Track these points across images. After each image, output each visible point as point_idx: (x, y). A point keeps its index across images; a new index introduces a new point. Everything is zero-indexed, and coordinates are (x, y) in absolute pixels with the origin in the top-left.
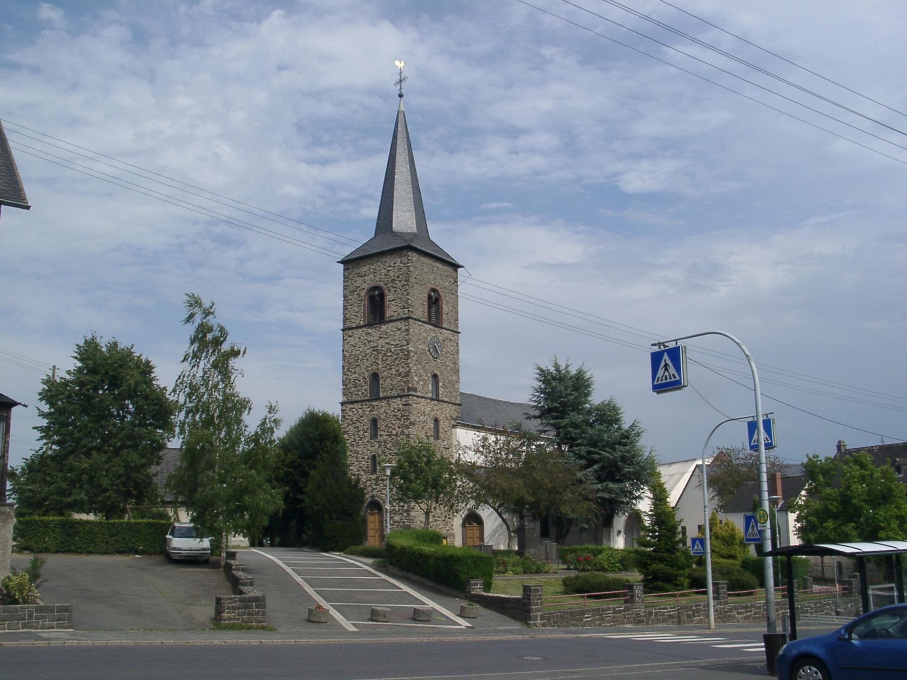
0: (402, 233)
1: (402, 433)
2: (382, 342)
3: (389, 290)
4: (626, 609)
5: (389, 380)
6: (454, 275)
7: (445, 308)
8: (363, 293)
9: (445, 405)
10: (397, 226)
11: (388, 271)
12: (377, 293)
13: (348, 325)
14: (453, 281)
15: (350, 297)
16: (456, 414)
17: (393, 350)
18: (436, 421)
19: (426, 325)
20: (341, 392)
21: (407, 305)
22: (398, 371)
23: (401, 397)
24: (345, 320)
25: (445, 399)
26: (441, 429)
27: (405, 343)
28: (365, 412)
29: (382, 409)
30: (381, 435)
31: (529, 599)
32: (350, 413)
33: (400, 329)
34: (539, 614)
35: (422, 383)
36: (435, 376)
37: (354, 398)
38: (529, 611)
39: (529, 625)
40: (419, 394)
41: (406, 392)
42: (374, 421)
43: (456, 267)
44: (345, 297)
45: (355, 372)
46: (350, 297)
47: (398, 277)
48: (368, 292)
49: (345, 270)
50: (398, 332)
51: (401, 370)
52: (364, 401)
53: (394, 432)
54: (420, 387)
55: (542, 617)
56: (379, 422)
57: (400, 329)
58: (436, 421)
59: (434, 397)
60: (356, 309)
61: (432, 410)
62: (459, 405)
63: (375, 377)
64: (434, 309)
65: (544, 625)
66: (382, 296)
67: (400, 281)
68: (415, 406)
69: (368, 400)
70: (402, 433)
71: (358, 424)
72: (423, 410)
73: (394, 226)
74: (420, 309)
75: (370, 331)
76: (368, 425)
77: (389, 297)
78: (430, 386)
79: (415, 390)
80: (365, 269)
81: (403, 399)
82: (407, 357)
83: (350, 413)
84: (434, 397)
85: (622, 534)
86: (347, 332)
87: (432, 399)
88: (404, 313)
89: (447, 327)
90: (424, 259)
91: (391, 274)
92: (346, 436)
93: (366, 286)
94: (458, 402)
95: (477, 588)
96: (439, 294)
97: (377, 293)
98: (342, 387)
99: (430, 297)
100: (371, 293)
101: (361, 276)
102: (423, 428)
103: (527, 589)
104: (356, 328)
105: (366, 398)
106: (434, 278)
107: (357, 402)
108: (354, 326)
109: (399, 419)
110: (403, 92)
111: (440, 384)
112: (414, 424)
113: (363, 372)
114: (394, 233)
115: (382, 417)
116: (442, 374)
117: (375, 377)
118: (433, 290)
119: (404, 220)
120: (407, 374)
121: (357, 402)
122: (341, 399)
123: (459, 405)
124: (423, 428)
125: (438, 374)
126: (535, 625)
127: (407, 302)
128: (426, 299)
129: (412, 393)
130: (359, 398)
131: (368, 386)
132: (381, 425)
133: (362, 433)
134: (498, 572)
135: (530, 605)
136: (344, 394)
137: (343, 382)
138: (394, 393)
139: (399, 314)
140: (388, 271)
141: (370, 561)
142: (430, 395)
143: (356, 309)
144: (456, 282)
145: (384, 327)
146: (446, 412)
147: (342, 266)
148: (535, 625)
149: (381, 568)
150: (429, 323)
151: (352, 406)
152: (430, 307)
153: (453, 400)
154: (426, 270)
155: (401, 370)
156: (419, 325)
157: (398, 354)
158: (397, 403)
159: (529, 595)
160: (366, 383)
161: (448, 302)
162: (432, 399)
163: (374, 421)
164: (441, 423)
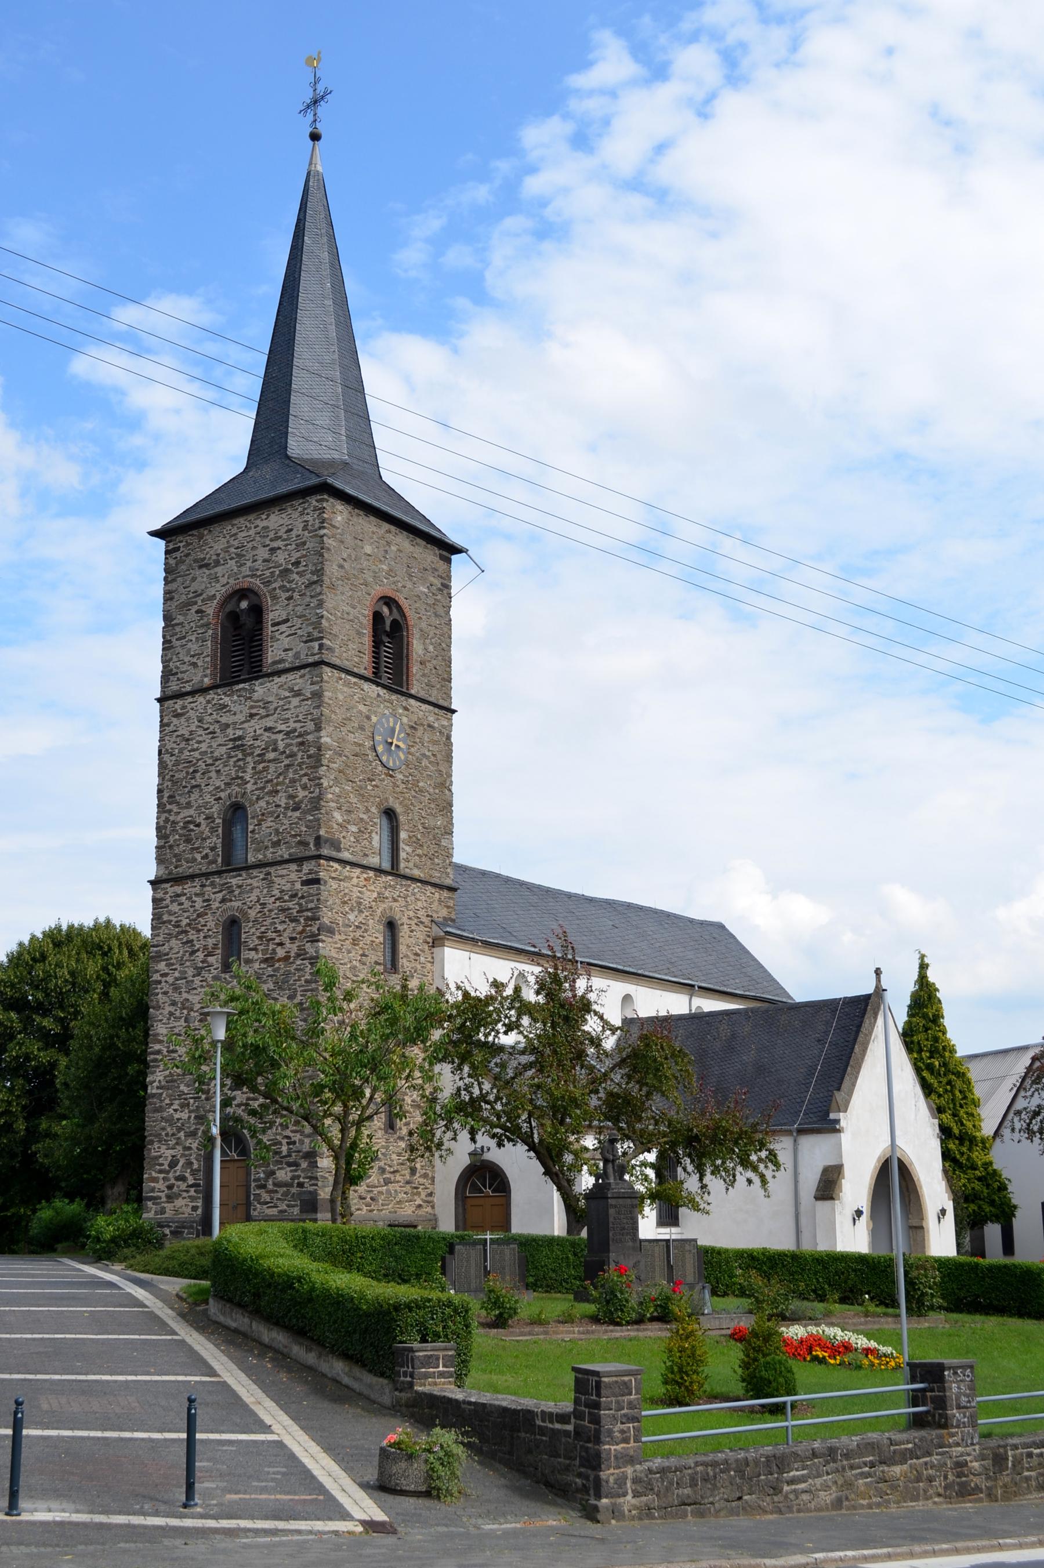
0: (314, 462)
1: (301, 954)
2: (256, 726)
3: (274, 598)
4: (922, 1450)
5: (269, 822)
6: (441, 565)
7: (417, 647)
8: (211, 609)
9: (415, 887)
10: (295, 447)
11: (273, 550)
12: (244, 605)
13: (174, 686)
14: (437, 582)
15: (180, 619)
16: (444, 913)
17: (281, 745)
18: (391, 926)
19: (366, 686)
20: (152, 853)
21: (316, 636)
22: (291, 797)
23: (299, 860)
24: (167, 675)
25: (416, 873)
26: (402, 949)
27: (311, 726)
28: (208, 904)
29: (252, 893)
30: (248, 961)
31: (596, 1420)
32: (175, 907)
33: (298, 694)
34: (629, 1470)
35: (354, 829)
36: (390, 814)
37: (184, 869)
38: (594, 1462)
39: (591, 1514)
40: (346, 855)
41: (312, 850)
42: (232, 926)
43: (448, 549)
44: (167, 618)
45: (189, 805)
46: (180, 619)
47: (297, 564)
48: (223, 604)
49: (167, 552)
50: (295, 701)
51: (301, 794)
52: (207, 875)
53: (281, 953)
54: (348, 840)
55: (643, 1486)
56: (246, 927)
57: (298, 694)
58: (391, 926)
59: (386, 865)
60: (194, 647)
61: (381, 898)
62: (452, 889)
63: (236, 811)
64: (386, 651)
65: (646, 1512)
66: (257, 611)
67: (301, 574)
68: (334, 885)
69: (219, 873)
70: (301, 954)
71: (192, 935)
72: (353, 899)
73: (292, 442)
74: (351, 642)
75: (226, 700)
76: (216, 939)
77: (273, 614)
78: (376, 838)
79: (336, 846)
80: (219, 547)
81: (306, 867)
82: (316, 761)
83: (175, 907)
84: (386, 865)
85: (864, 1218)
86: (167, 704)
87: (379, 871)
88: (306, 653)
89: (422, 694)
90: (369, 525)
91: (281, 557)
92: (162, 966)
93: (219, 591)
94: (448, 882)
95: (437, 1382)
96: (399, 608)
97: (244, 605)
98: (154, 841)
99: (377, 617)
100: (229, 608)
101: (207, 566)
102: (355, 942)
103: (587, 1384)
104: (192, 693)
105: (213, 868)
106: (390, 572)
107: (192, 877)
108: (188, 688)
109: (294, 920)
110: (321, 128)
111: (403, 835)
112: (331, 931)
113: (207, 803)
114: (288, 458)
115: (252, 914)
116: (407, 810)
117: (236, 811)
118: (388, 601)
119: (312, 438)
120: (316, 803)
121: (192, 877)
122: (151, 871)
123: (452, 889)
124: (355, 942)
125: (399, 809)
126: (616, 1512)
127: (317, 625)
128: (367, 622)
129: (325, 851)
130: (195, 869)
131: (221, 830)
132: (250, 934)
133: (200, 955)
134: (1008, 1247)
135: (598, 1440)
136: (160, 860)
137: (159, 829)
138: (284, 853)
139: (297, 655)
140: (273, 550)
141: (175, 1285)
142: (374, 861)
143: (194, 647)
144: (448, 587)
145: (261, 689)
146: (415, 906)
147: (161, 544)
148: (616, 1512)
149: (192, 1309)
150: (375, 679)
151: (178, 889)
152: (377, 644)
153: (436, 877)
154: (368, 549)
155: (301, 794)
156: (347, 684)
157: (292, 755)
158: (289, 878)
159: (597, 1405)
160: (213, 830)
161: (424, 636)
162: (379, 871)
163: (232, 926)
164: (404, 932)
